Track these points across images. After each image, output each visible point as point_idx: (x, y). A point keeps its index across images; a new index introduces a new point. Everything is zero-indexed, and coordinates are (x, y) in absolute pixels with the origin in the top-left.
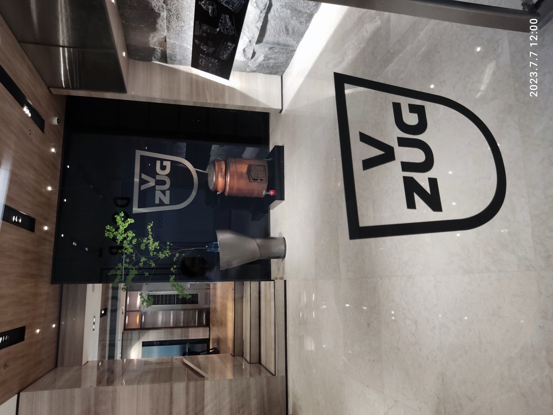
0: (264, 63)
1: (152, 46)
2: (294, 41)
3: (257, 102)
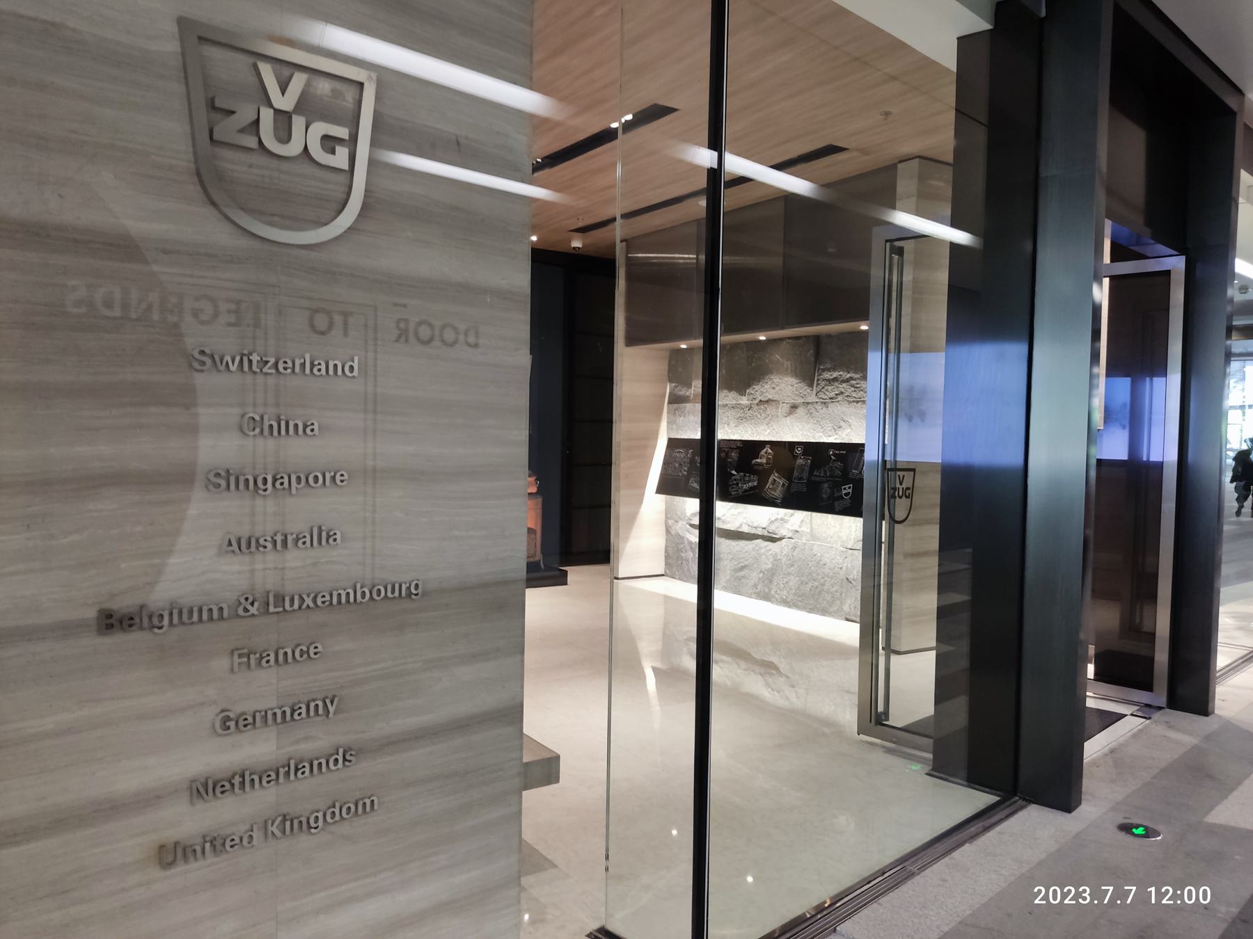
0: (686, 542)
1: (693, 384)
2: (726, 582)
3: (627, 538)
